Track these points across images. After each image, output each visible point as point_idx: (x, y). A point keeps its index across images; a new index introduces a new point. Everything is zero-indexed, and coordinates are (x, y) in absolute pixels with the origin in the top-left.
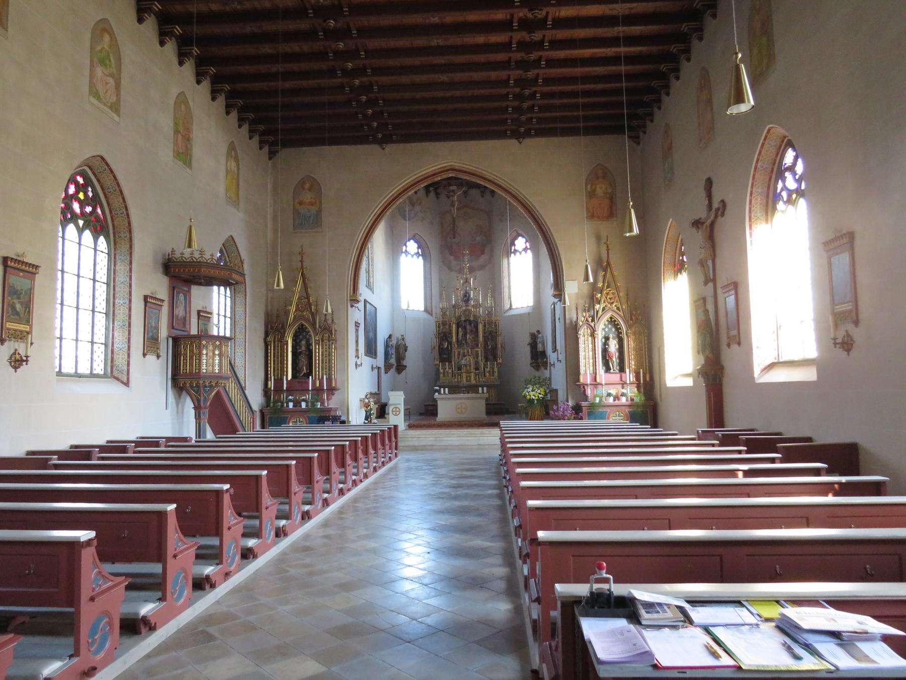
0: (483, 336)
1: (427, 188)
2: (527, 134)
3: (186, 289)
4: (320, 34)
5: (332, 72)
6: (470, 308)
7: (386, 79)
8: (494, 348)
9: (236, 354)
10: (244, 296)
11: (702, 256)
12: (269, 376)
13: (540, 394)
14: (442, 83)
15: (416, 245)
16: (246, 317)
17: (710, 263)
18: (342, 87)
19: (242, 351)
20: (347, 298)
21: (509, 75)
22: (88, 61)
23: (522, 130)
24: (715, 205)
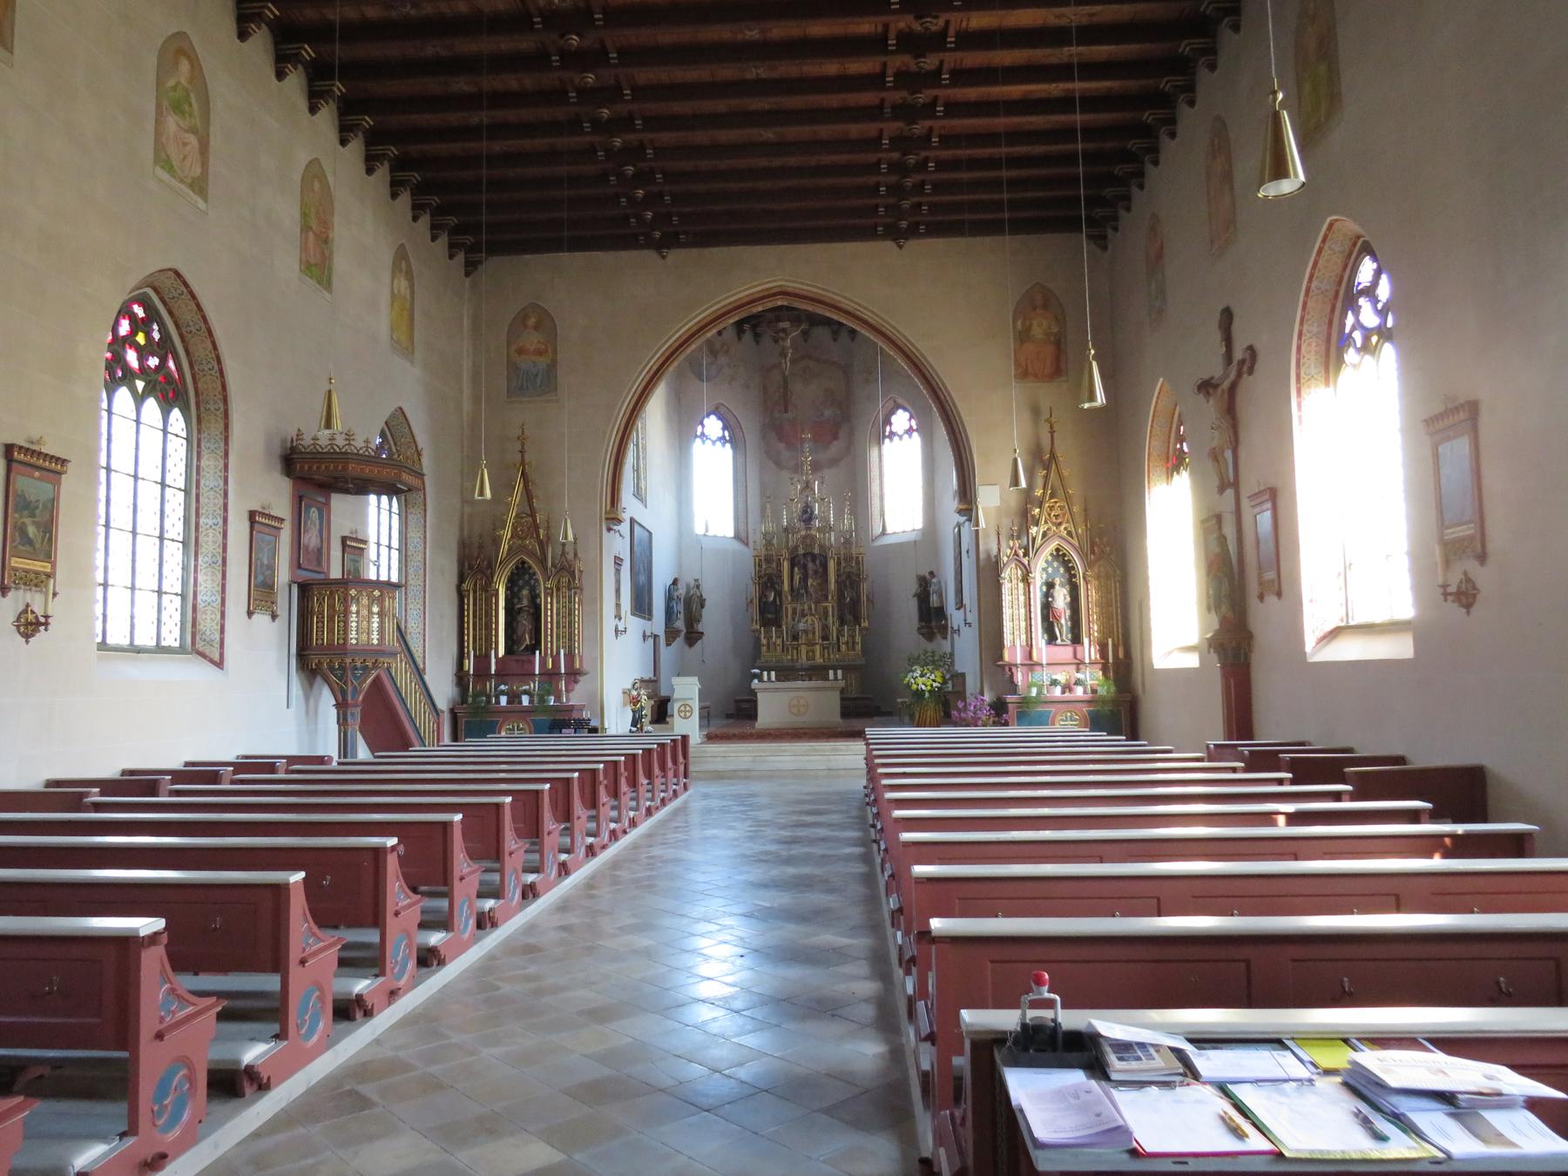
0: (836, 581)
1: (739, 325)
2: (913, 232)
3: (321, 499)
4: (554, 58)
5: (574, 125)
6: (813, 532)
7: (667, 137)
8: (856, 602)
9: (409, 612)
10: (422, 512)
11: (1215, 443)
12: (466, 650)
13: (934, 681)
14: (765, 144)
15: (720, 424)
16: (425, 548)
17: (1229, 454)
18: (591, 150)
19: (419, 606)
20: (601, 516)
21: (881, 130)
22: (152, 106)
23: (904, 224)
24: (1238, 354)
